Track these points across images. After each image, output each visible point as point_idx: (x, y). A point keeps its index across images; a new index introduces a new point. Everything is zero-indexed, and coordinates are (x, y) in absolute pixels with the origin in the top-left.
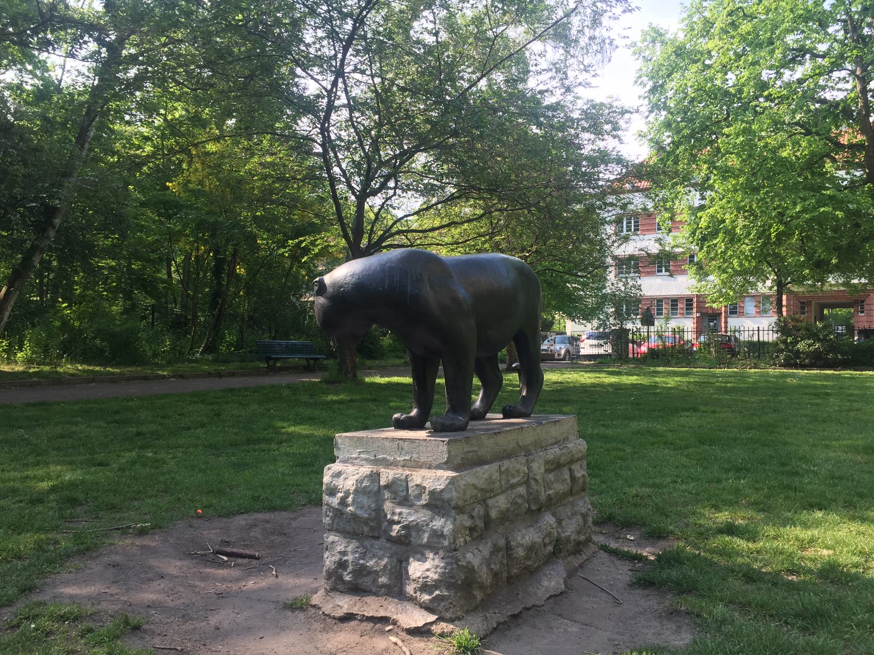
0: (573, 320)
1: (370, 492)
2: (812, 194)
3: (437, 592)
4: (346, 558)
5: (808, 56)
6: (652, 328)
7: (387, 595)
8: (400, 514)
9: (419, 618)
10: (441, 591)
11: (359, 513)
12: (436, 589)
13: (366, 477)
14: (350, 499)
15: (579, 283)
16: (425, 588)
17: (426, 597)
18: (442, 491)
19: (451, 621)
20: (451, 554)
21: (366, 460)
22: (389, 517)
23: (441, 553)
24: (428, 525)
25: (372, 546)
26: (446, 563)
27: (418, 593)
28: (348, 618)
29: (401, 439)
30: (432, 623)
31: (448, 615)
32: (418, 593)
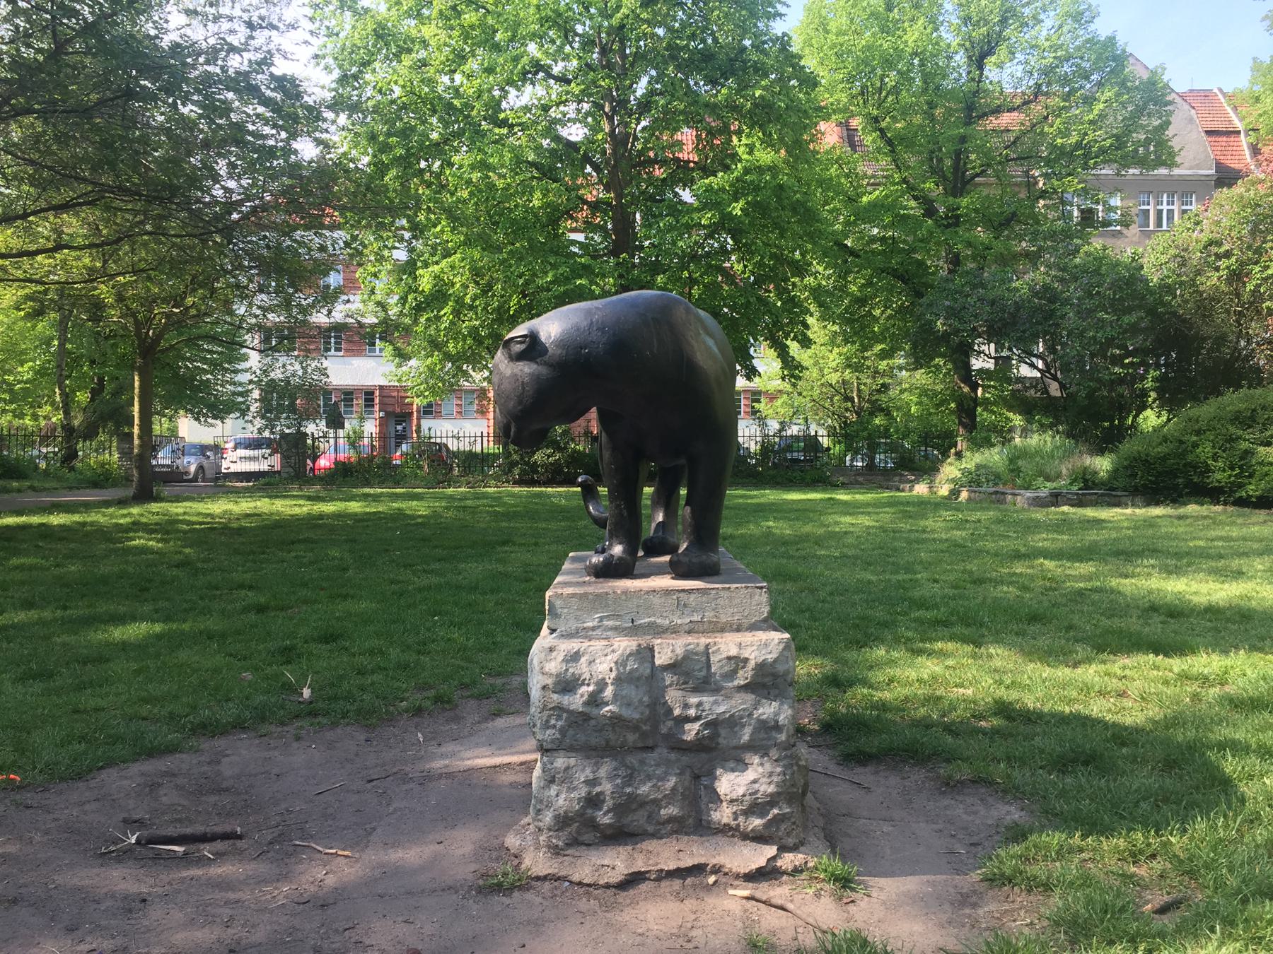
0: (197, 419)
1: (638, 679)
2: (564, 260)
3: (776, 811)
4: (598, 789)
5: (541, 75)
6: (341, 433)
7: (676, 832)
8: (699, 704)
9: (759, 856)
10: (780, 808)
11: (627, 713)
12: (772, 807)
13: (630, 655)
14: (609, 692)
15: (204, 361)
16: (755, 808)
17: (757, 822)
18: (776, 660)
19: (794, 849)
20: (789, 753)
21: (615, 628)
22: (677, 712)
23: (774, 753)
24: (750, 715)
25: (642, 762)
26: (784, 766)
27: (741, 819)
28: (633, 880)
29: (683, 591)
30: (774, 858)
31: (790, 841)
32: (741, 819)
